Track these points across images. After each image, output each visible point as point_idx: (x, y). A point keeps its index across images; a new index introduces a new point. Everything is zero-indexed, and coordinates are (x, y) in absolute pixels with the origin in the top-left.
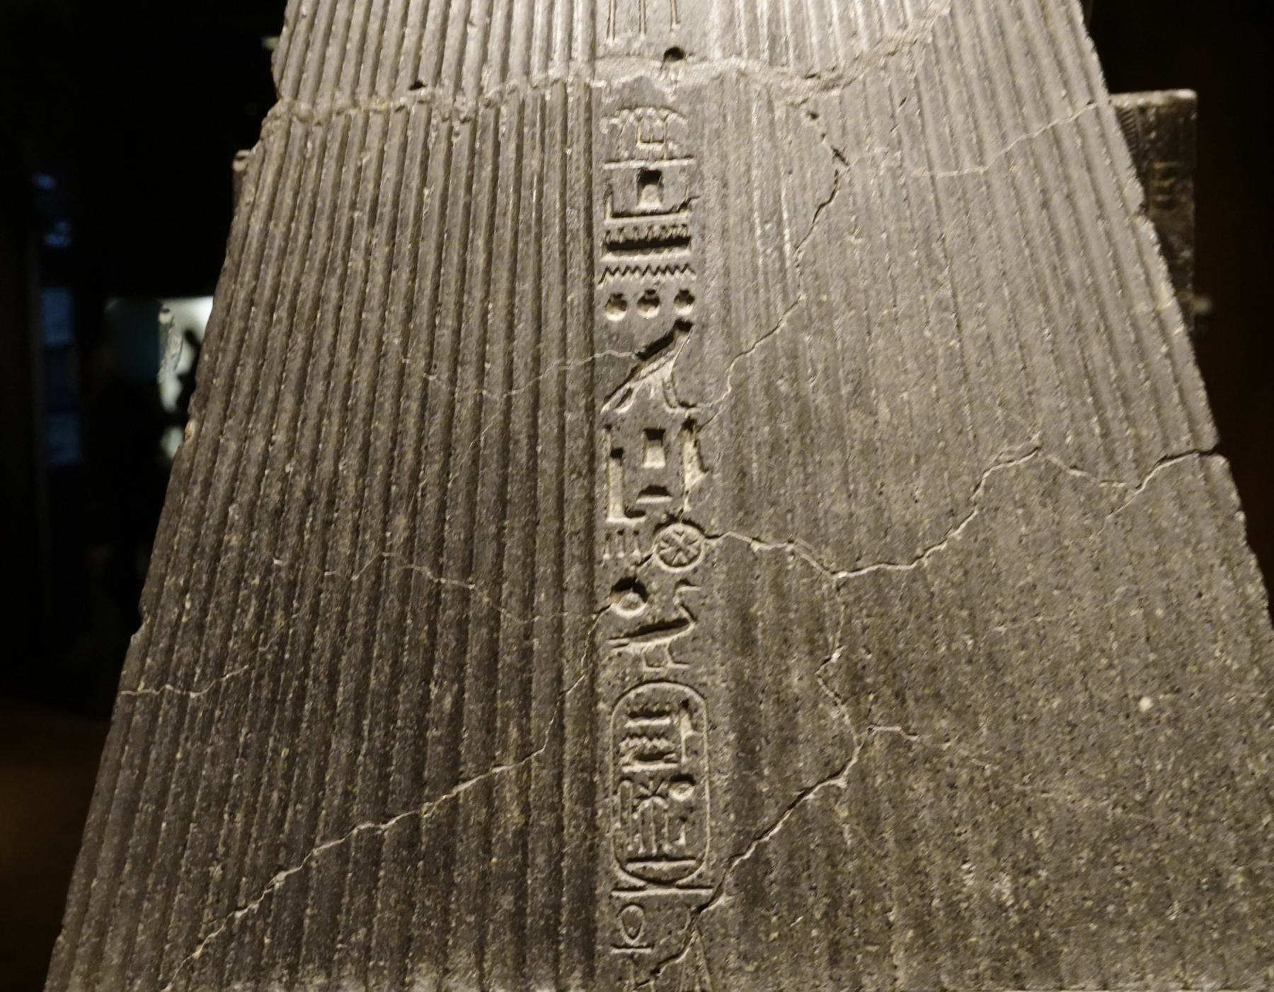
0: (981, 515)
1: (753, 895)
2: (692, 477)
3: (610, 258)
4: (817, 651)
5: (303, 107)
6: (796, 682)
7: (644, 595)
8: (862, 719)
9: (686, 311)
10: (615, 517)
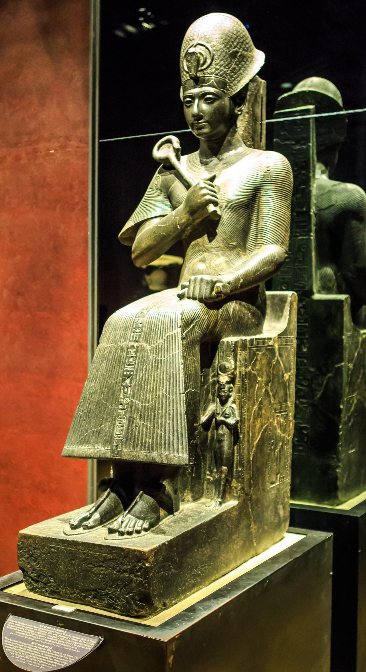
0: (88, 564)
1: (127, 440)
3: (126, 366)
4: (137, 413)
6: (135, 416)
8: (140, 421)
9: (132, 373)
10: (121, 396)
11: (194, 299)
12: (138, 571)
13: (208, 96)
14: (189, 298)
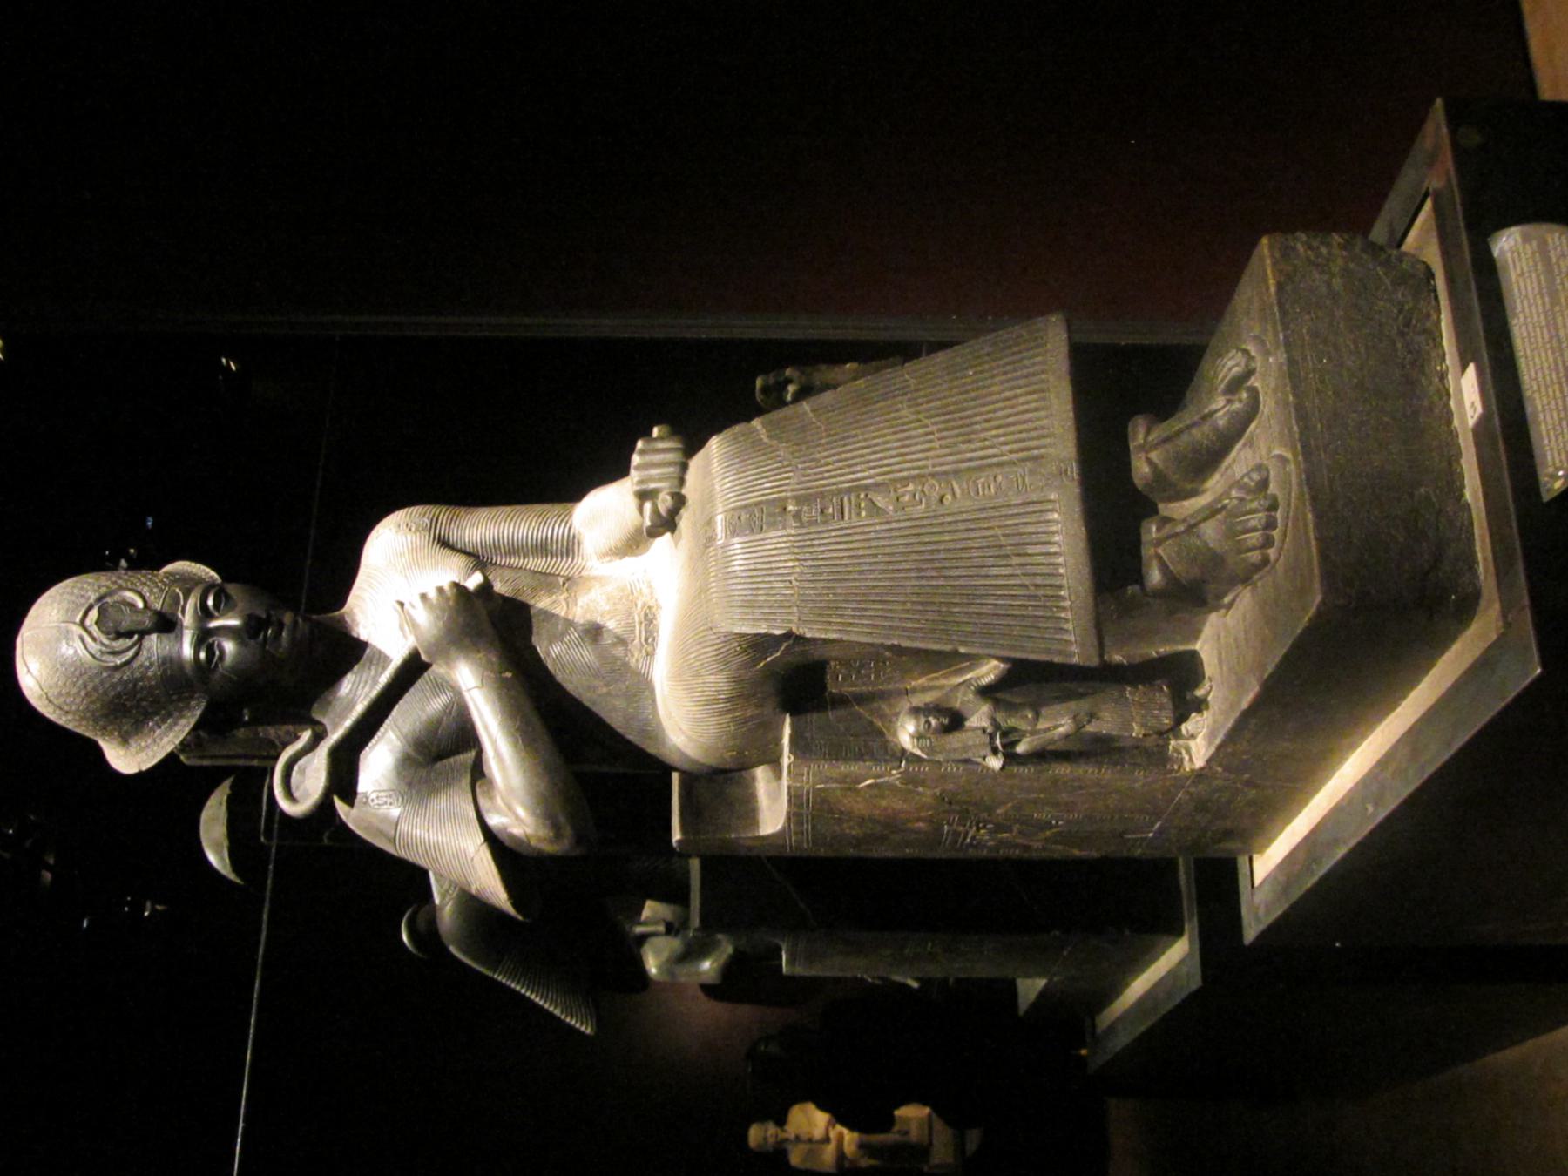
2: (911, 487)
5: (795, 618)
7: (942, 497)
11: (684, 467)
12: (1319, 255)
13: (210, 602)
14: (682, 481)
